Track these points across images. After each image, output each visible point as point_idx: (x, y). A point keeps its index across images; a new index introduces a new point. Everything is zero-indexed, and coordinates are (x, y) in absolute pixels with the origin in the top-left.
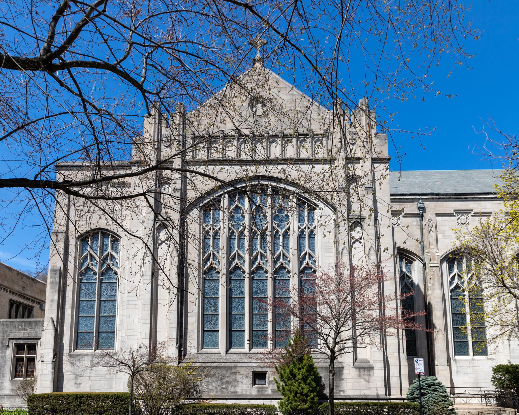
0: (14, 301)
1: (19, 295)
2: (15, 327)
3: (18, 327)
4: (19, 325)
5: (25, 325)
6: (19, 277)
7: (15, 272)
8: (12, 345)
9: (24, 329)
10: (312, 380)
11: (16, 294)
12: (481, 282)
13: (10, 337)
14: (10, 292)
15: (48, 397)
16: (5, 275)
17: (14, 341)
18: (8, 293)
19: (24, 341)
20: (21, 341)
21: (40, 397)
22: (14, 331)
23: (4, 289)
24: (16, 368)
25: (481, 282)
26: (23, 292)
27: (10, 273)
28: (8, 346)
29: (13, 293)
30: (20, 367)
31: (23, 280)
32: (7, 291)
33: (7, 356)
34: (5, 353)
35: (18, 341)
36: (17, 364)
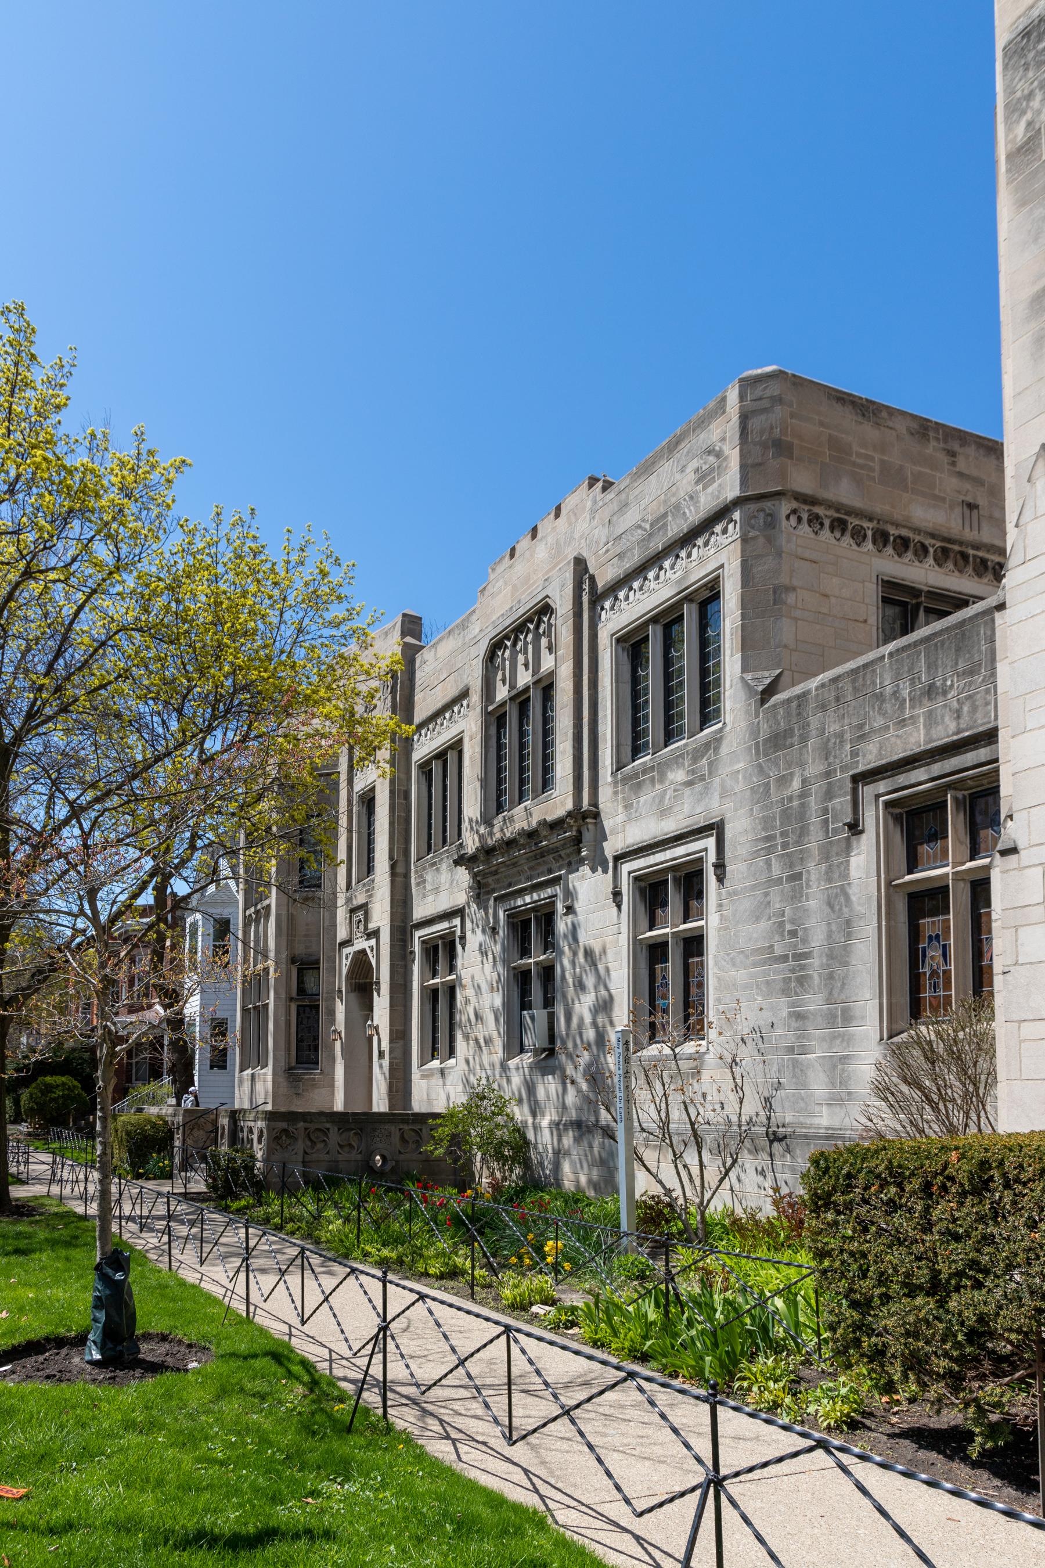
0: (914, 592)
1: (943, 556)
2: (880, 697)
3: (895, 693)
4: (897, 678)
5: (931, 666)
6: (933, 448)
7: (901, 426)
8: (872, 817)
9: (930, 692)
10: (932, 1233)
11: (922, 551)
12: (119, 1530)
13: (861, 768)
14: (882, 538)
15: (980, 1186)
16: (834, 444)
17: (882, 786)
18: (869, 545)
19: (937, 769)
20: (920, 774)
21: (897, 1176)
22: (879, 722)
23: (839, 525)
24: (915, 958)
25: (119, 1530)
26: (969, 535)
27: (870, 432)
28: (855, 828)
29: (903, 545)
30: (934, 953)
31: (962, 465)
32: (859, 536)
33: (854, 892)
34: (845, 876)
35: (902, 779)
36: (914, 933)
